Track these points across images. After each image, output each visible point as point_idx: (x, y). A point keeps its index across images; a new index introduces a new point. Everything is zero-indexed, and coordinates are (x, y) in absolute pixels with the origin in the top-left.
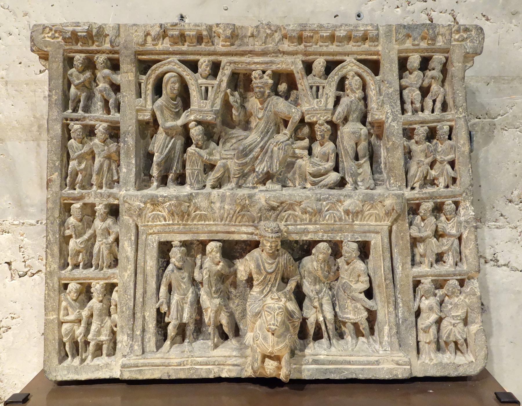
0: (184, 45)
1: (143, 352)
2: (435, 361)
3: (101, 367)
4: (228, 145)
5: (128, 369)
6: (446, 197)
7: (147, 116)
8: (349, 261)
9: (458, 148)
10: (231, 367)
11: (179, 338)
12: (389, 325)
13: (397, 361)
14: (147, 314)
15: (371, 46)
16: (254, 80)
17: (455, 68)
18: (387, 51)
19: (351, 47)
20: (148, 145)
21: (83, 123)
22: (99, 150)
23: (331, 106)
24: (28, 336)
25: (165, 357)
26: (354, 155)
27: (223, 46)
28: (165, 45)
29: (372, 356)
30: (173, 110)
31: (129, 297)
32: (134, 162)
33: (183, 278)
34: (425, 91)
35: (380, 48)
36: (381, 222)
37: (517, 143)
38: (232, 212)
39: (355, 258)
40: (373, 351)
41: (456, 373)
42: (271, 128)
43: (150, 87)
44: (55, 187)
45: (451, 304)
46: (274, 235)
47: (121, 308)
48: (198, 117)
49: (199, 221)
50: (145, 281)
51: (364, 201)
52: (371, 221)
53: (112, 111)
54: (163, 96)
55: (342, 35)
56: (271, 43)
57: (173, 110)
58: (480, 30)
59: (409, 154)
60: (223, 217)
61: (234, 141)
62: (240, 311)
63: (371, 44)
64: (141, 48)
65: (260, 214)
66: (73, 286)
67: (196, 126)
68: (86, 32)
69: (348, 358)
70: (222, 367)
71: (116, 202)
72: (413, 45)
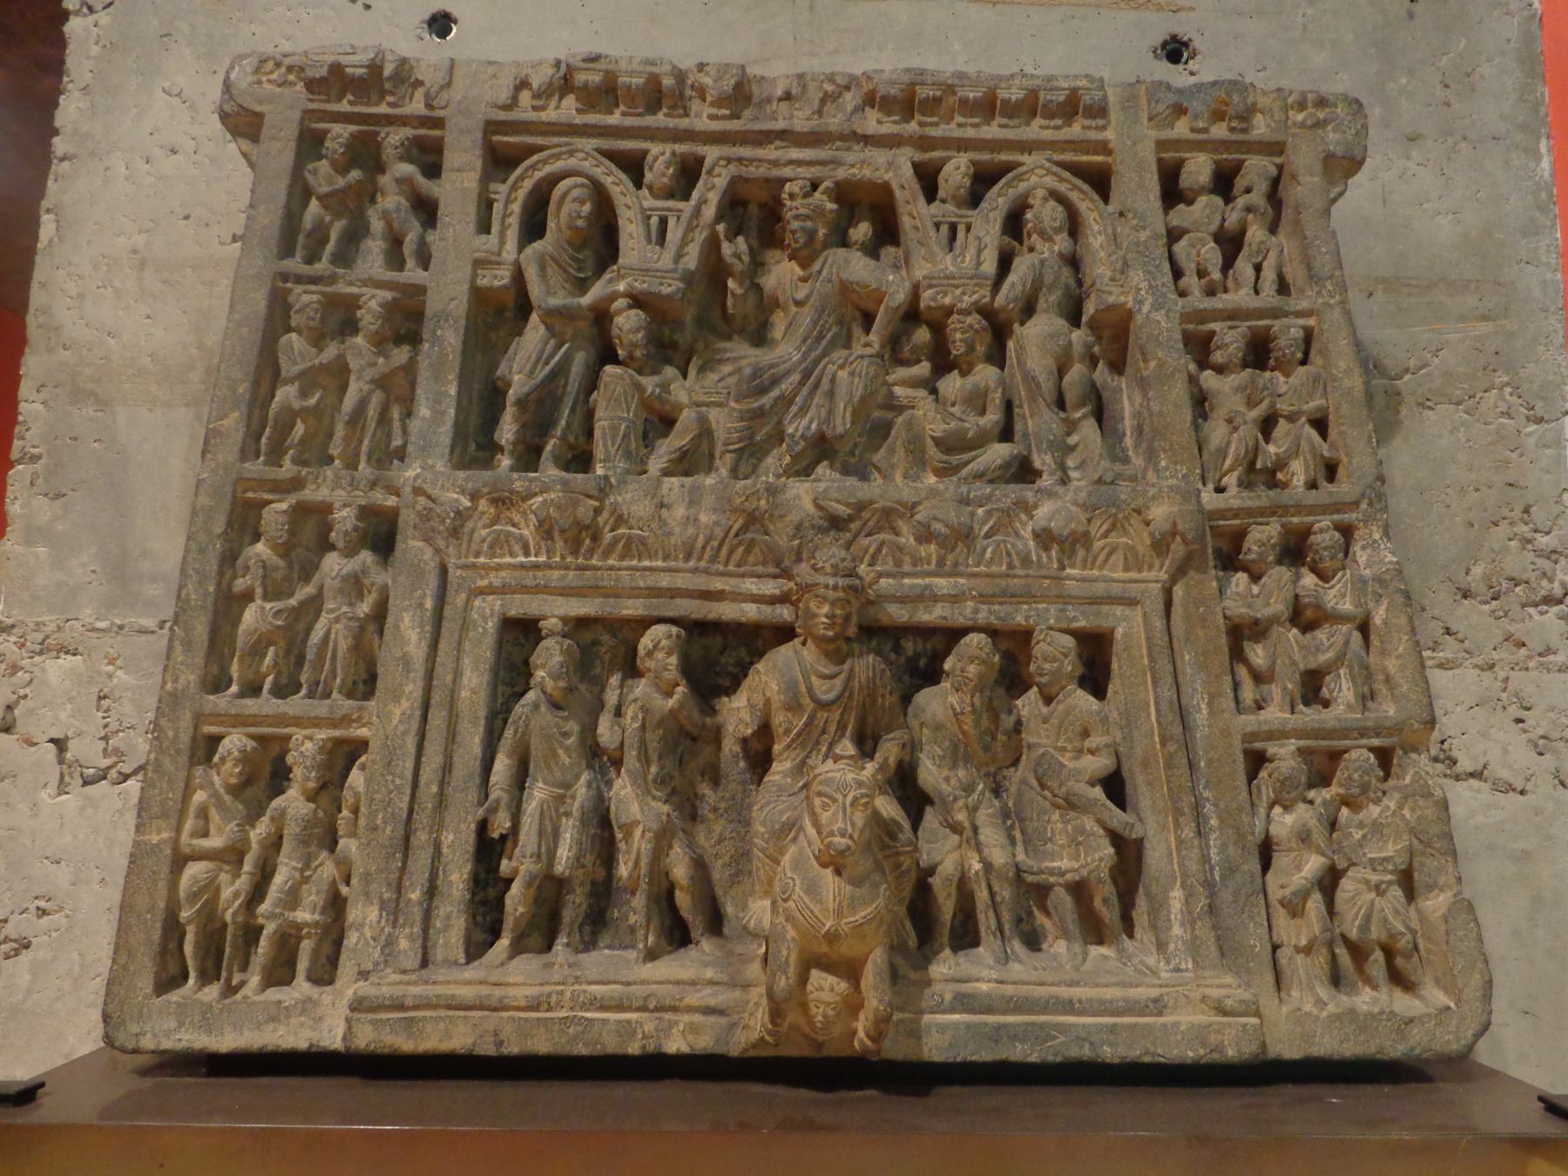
0: (611, 113)
1: (425, 963)
2: (1331, 1008)
3: (287, 1008)
4: (712, 377)
5: (370, 1016)
6: (1312, 510)
7: (498, 278)
8: (1054, 690)
9: (1334, 380)
10: (697, 1018)
11: (535, 939)
12: (1183, 886)
13: (1219, 1001)
14: (448, 838)
15: (1089, 128)
16: (788, 203)
17: (1306, 186)
18: (1128, 142)
19: (1036, 129)
20: (496, 366)
21: (329, 289)
22: (363, 363)
23: (990, 266)
24: (77, 969)
25: (493, 979)
26: (1055, 394)
27: (712, 117)
28: (567, 109)
29: (1137, 986)
30: (571, 271)
31: (398, 781)
32: (453, 391)
33: (566, 735)
34: (1231, 244)
35: (1109, 134)
36: (1140, 571)
37: (1464, 440)
38: (719, 532)
39: (1070, 677)
40: (1141, 972)
41: (1401, 1047)
42: (830, 329)
43: (516, 207)
44: (227, 453)
45: (1361, 825)
46: (841, 582)
47: (372, 815)
48: (636, 284)
49: (622, 558)
50: (452, 735)
51: (1090, 508)
52: (1114, 568)
53: (410, 263)
54: (548, 234)
55: (1014, 98)
56: (834, 116)
57: (571, 271)
58: (1357, 106)
59: (1201, 403)
60: (693, 547)
61: (727, 369)
62: (727, 859)
63: (1087, 122)
64: (503, 116)
65: (797, 542)
66: (234, 742)
67: (630, 307)
68: (368, 67)
69: (1065, 992)
70: (668, 1016)
71: (392, 501)
72: (1193, 130)
